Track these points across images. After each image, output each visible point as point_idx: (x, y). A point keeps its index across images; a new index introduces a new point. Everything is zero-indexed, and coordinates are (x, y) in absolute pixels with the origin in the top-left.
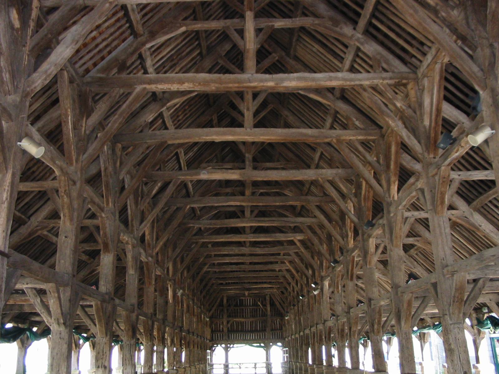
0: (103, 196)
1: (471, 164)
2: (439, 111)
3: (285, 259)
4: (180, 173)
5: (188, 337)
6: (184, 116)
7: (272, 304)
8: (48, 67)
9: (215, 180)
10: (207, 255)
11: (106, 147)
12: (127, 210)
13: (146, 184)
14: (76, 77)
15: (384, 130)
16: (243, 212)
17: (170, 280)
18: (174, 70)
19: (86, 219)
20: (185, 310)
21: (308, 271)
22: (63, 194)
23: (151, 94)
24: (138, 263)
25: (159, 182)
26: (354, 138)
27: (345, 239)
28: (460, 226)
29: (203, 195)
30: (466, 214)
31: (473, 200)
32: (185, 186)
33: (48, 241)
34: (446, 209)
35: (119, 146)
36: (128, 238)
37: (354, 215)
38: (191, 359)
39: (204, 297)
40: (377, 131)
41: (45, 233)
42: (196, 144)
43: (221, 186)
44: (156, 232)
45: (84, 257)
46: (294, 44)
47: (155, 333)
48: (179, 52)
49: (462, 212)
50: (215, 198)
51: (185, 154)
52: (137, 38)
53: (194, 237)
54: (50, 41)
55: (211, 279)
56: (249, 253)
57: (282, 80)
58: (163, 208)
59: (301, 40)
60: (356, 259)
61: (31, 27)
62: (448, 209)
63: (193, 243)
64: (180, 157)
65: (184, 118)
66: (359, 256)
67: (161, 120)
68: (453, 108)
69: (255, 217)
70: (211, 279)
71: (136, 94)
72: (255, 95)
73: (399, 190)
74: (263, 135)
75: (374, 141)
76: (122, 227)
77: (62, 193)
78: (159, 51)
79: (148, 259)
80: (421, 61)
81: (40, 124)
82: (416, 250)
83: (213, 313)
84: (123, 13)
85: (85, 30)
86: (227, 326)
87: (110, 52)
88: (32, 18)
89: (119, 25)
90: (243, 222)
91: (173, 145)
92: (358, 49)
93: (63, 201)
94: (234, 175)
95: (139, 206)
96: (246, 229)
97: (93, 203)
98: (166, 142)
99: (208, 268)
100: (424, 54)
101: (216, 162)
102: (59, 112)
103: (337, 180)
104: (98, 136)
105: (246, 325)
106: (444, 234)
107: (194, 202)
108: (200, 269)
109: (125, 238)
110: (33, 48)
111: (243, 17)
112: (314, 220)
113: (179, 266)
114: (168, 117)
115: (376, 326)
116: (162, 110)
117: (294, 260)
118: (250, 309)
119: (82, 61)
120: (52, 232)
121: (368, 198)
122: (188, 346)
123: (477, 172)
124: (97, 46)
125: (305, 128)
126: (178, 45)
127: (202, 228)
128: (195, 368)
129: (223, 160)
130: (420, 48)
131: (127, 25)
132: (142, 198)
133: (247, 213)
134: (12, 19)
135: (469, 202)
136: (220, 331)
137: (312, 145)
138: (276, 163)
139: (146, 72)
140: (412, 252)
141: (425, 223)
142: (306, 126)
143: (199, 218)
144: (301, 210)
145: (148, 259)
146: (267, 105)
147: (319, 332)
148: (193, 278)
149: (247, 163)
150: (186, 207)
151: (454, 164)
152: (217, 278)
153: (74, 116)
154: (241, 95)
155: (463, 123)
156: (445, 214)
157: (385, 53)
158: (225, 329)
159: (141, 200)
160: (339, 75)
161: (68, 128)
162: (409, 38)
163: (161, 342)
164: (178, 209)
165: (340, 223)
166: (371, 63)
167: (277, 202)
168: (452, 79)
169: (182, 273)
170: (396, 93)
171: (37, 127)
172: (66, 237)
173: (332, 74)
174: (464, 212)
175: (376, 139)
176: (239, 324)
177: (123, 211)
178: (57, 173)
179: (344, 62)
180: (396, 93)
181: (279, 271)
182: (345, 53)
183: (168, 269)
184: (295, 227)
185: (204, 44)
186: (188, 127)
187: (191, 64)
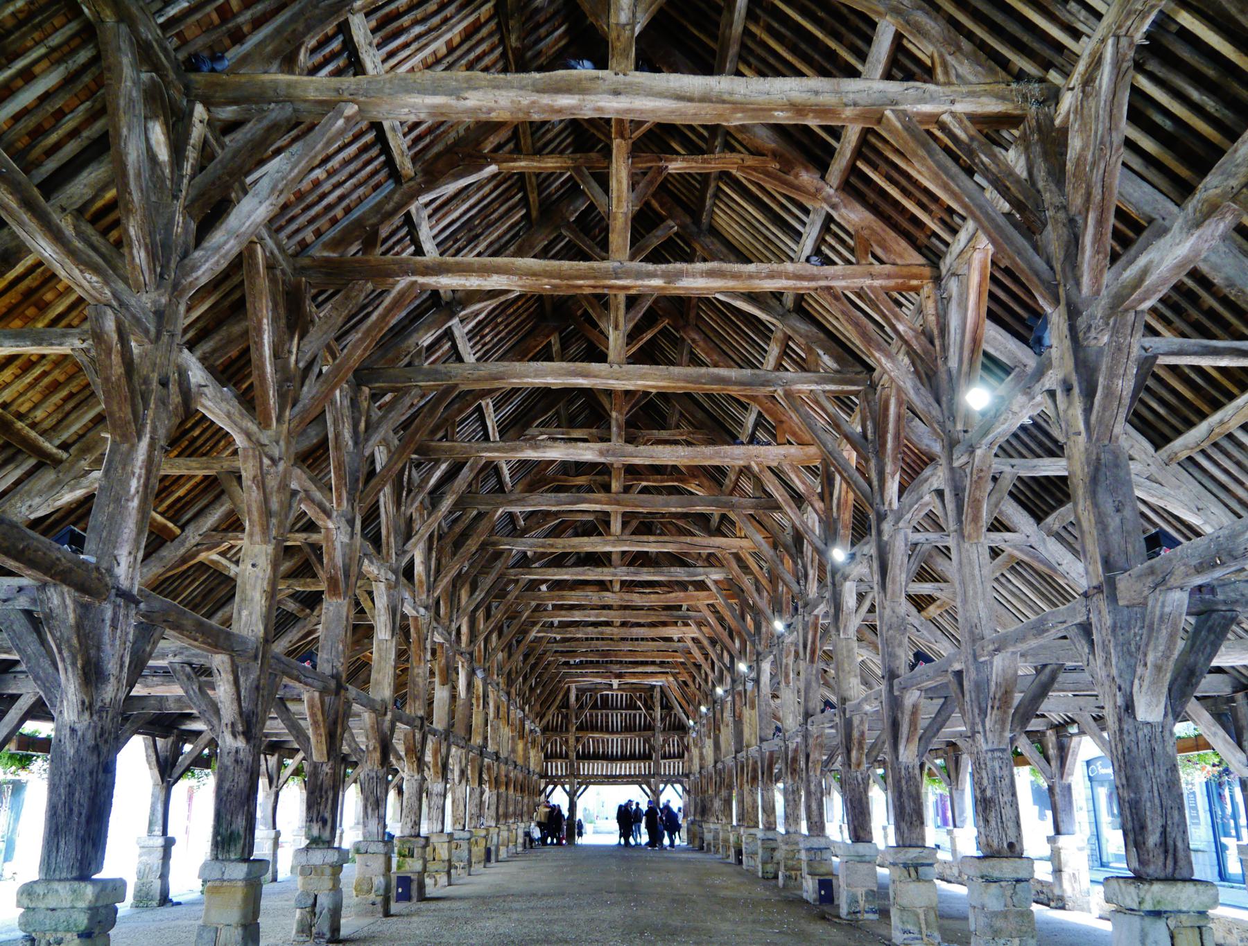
1: (1041, 444)
2: (976, 341)
3: (689, 617)
4: (485, 445)
8: (223, 239)
9: (553, 462)
10: (538, 606)
11: (338, 392)
12: (378, 516)
14: (280, 257)
15: (876, 374)
16: (608, 524)
17: (461, 654)
19: (297, 531)
20: (491, 715)
21: (734, 642)
22: (250, 483)
26: (819, 387)
27: (802, 582)
29: (532, 488)
30: (1032, 541)
31: (1047, 514)
32: (497, 470)
33: (221, 574)
34: (984, 529)
36: (379, 570)
39: (532, 689)
41: (215, 557)
42: (515, 391)
43: (566, 473)
45: (291, 606)
46: (708, 202)
47: (428, 757)
48: (484, 212)
51: (497, 408)
52: (401, 184)
54: (228, 188)
55: (545, 652)
57: (679, 275)
58: (451, 512)
59: (722, 196)
60: (821, 621)
61: (191, 161)
62: (989, 530)
68: (1008, 336)
69: (633, 533)
70: (545, 652)
72: (632, 301)
73: (902, 490)
74: (642, 377)
75: (856, 394)
76: (370, 549)
78: (446, 209)
80: (947, 244)
81: (207, 346)
82: (939, 607)
84: (374, 133)
85: (296, 171)
87: (348, 210)
88: (192, 141)
89: (365, 157)
90: (606, 543)
92: (829, 219)
93: (249, 497)
94: (587, 453)
96: (614, 557)
97: (309, 498)
100: (954, 231)
101: (558, 426)
102: (244, 324)
103: (787, 469)
106: (978, 577)
107: (511, 503)
108: (524, 632)
109: (370, 568)
110: (193, 201)
111: (607, 152)
115: (854, 754)
119: (294, 227)
121: (846, 501)
122: (496, 783)
123: (1047, 461)
124: (323, 196)
126: (484, 198)
127: (529, 553)
128: (509, 830)
129: (572, 423)
130: (947, 219)
131: (382, 158)
133: (616, 526)
134: (153, 142)
135: (1038, 517)
136: (561, 757)
137: (742, 399)
139: (419, 251)
140: (932, 610)
143: (523, 533)
144: (721, 522)
151: (1000, 447)
153: (276, 330)
154: (602, 301)
156: (982, 539)
157: (878, 225)
158: (573, 755)
159: (407, 495)
160: (789, 266)
161: (261, 356)
162: (925, 200)
164: (480, 516)
165: (793, 550)
166: (852, 243)
167: (671, 506)
168: (1007, 282)
169: (487, 640)
170: (900, 305)
171: (199, 353)
172: (254, 565)
173: (775, 266)
177: (371, 516)
178: (240, 441)
179: (802, 241)
182: (804, 224)
183: (459, 630)
184: (710, 555)
185: (533, 197)
187: (508, 236)
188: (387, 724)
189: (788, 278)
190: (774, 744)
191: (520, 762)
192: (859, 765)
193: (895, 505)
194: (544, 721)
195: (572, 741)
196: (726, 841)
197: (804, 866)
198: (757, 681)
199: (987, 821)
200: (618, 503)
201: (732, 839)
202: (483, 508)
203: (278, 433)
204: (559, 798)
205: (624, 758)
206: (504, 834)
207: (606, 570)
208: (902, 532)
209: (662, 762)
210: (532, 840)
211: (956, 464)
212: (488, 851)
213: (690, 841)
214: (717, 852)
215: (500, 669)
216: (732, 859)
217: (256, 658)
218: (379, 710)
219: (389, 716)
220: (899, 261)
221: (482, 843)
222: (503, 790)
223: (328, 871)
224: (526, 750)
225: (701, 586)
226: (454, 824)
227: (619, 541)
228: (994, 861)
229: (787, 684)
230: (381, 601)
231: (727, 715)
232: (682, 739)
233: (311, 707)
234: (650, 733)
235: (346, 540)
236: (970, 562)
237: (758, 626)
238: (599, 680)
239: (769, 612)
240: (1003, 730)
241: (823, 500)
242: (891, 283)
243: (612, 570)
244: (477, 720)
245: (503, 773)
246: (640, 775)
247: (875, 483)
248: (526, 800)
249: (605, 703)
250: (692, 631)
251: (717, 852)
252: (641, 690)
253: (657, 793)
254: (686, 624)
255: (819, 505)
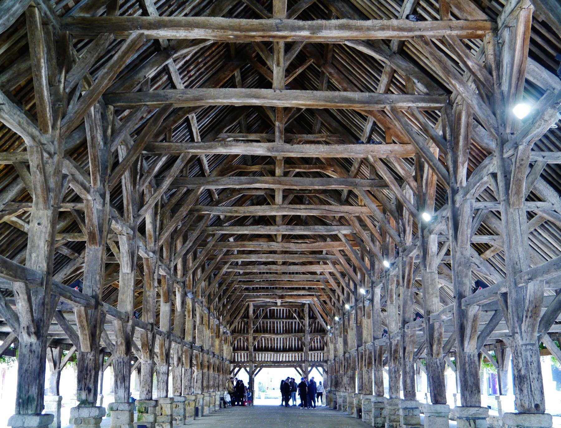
0: (89, 174)
2: (520, 72)
3: (328, 259)
4: (191, 144)
5: (201, 356)
6: (198, 71)
7: (312, 317)
9: (237, 155)
11: (92, 109)
13: (147, 158)
14: (51, 17)
15: (453, 96)
16: (273, 197)
18: (183, 10)
20: (198, 323)
22: (35, 169)
23: (152, 41)
24: (135, 258)
25: (164, 156)
28: (549, 223)
29: (222, 173)
32: (199, 161)
33: (19, 230)
35: (111, 108)
36: (122, 227)
37: (414, 206)
38: (205, 384)
39: (224, 306)
40: (445, 97)
41: (14, 219)
42: (211, 108)
43: (245, 163)
44: (160, 221)
45: (65, 251)
47: (157, 350)
49: (551, 205)
50: (237, 178)
53: (210, 228)
56: (281, 250)
57: (320, 28)
60: (414, 261)
63: (209, 235)
64: (192, 125)
65: (198, 74)
66: (417, 257)
67: (167, 76)
69: (290, 203)
71: (131, 42)
72: (289, 47)
74: (296, 98)
75: (439, 109)
77: (33, 168)
79: (148, 255)
80: (503, 6)
83: (235, 327)
86: (253, 343)
90: (272, 210)
91: (181, 109)
95: (137, 187)
96: (278, 219)
98: (171, 105)
99: (228, 268)
101: (240, 132)
103: (392, 160)
104: (83, 94)
105: (179, 135)
107: (209, 183)
109: (116, 226)
112: (364, 209)
113: (191, 265)
114: (175, 72)
116: (167, 63)
117: (339, 260)
118: (283, 322)
120: (23, 218)
125: (354, 91)
127: (222, 217)
128: (210, 396)
129: (249, 130)
132: (142, 175)
133: (279, 198)
136: (244, 350)
137: (363, 113)
138: (317, 135)
139: (145, 13)
140: (488, 254)
141: (497, 215)
142: (356, 89)
143: (217, 203)
144: (348, 196)
145: (148, 255)
146: (306, 60)
147: (367, 353)
148: (209, 280)
149: (277, 134)
150: (199, 189)
152: (240, 281)
153: (49, 68)
154: (268, 46)
155: (554, 89)
156: (522, 206)
158: (251, 348)
159: (140, 178)
160: (394, 22)
161: (40, 84)
163: (165, 361)
164: (189, 192)
167: (315, 185)
169: (194, 273)
172: (39, 224)
173: (385, 22)
174: (553, 204)
175: (442, 107)
176: (268, 340)
177: (117, 192)
178: (27, 141)
180: (470, 48)
181: (321, 274)
183: (176, 267)
186: (200, 87)
188: (129, 328)
189: (394, 30)
190: (382, 341)
191: (217, 353)
192: (438, 354)
193: (464, 184)
194: (233, 326)
195: (251, 339)
196: (351, 403)
197: (402, 419)
198: (372, 300)
199: (521, 390)
200: (280, 183)
201: (355, 402)
202: (190, 187)
203: (53, 136)
204: (243, 376)
205: (285, 350)
206: (207, 399)
207: (272, 227)
208: (469, 202)
209: (310, 353)
210: (225, 403)
211: (505, 156)
212: (197, 409)
213: (328, 403)
214: (345, 410)
215: (203, 292)
216: (355, 415)
217: (42, 284)
218: (124, 319)
219: (130, 323)
220: (469, 18)
221: (193, 404)
222: (206, 370)
223: (93, 421)
224: (221, 345)
225: (335, 238)
226: (174, 392)
227: (281, 208)
228: (526, 416)
229: (392, 302)
230: (124, 248)
231: (352, 323)
232: (323, 338)
233: (80, 316)
234: (302, 334)
235: (100, 207)
236: (514, 222)
237: (373, 265)
238: (268, 300)
239: (380, 255)
240: (533, 331)
241: (416, 180)
242: (464, 33)
243: (276, 227)
244: (188, 326)
245: (206, 360)
246: (295, 361)
247: (451, 169)
248: (221, 377)
249: (273, 315)
250: (330, 268)
251: (345, 410)
252: (296, 306)
253: (306, 373)
254: (325, 263)
255: (414, 184)
